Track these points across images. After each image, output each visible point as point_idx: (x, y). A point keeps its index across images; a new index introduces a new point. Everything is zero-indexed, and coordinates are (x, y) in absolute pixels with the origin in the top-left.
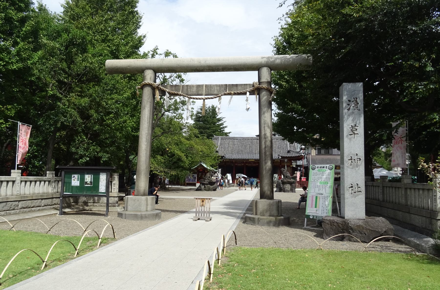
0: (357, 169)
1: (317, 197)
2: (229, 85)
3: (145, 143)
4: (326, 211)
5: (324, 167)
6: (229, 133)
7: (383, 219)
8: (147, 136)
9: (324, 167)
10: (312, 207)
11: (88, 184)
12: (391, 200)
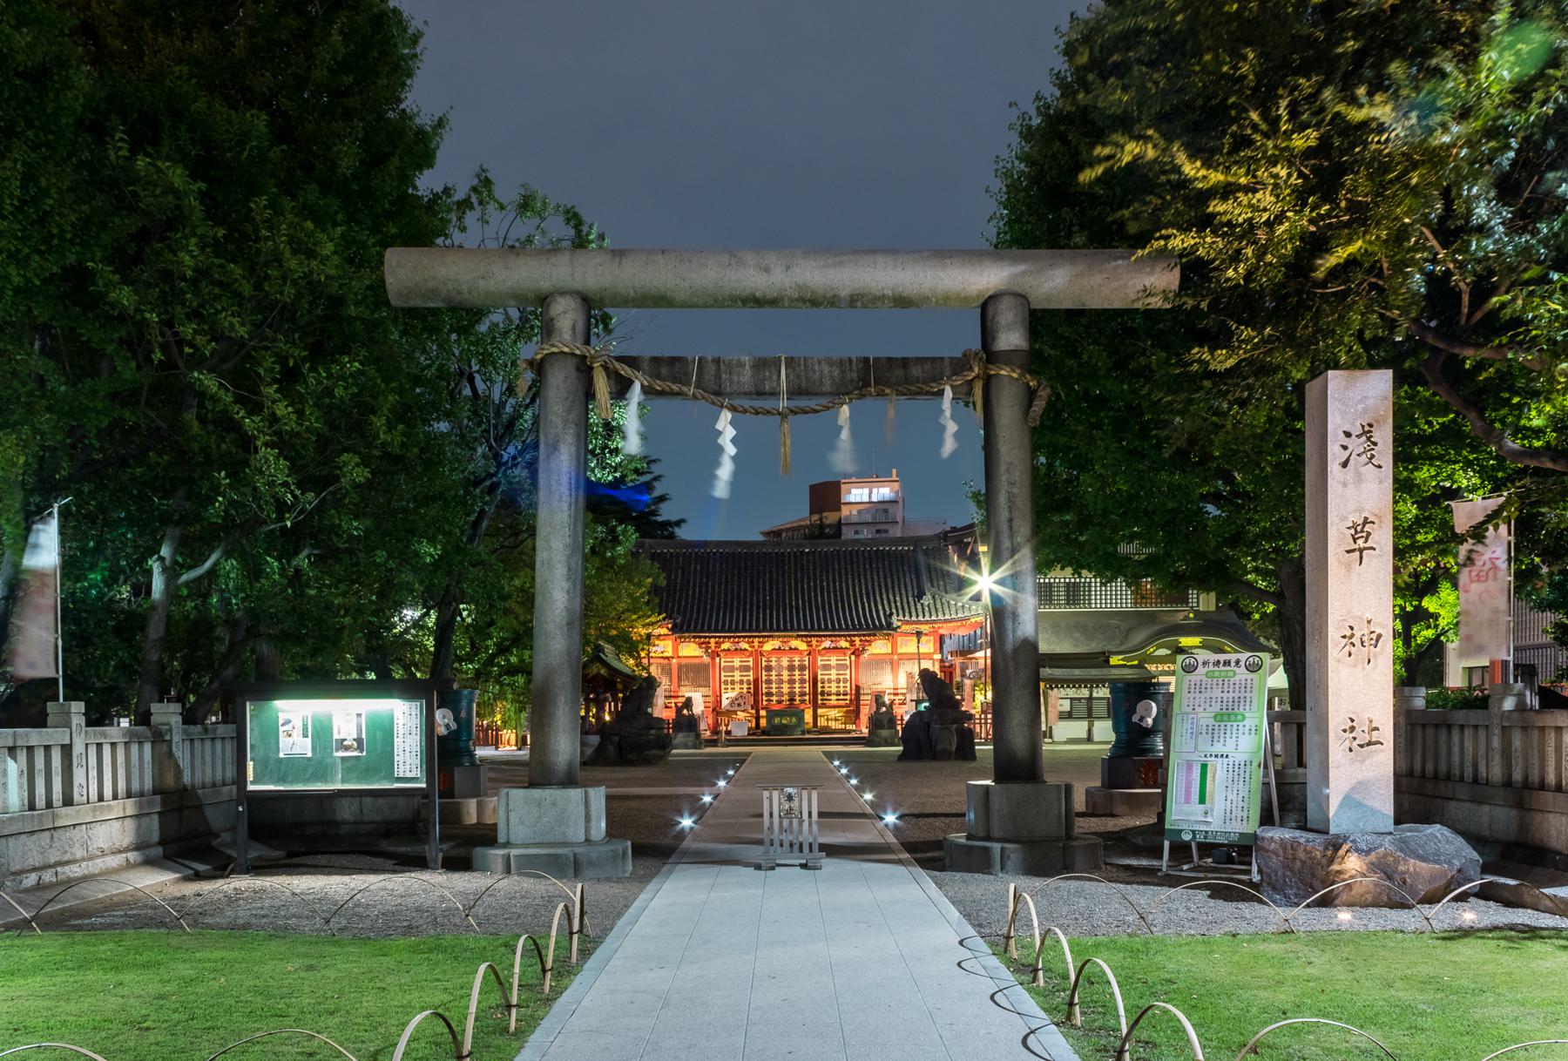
0: (1368, 668)
1: (1204, 767)
2: (877, 360)
3: (565, 585)
4: (1240, 814)
5: (1227, 663)
6: (679, 523)
7: (1446, 832)
8: (569, 557)
9: (1227, 663)
10: (1188, 801)
11: (347, 748)
12: (1443, 768)
